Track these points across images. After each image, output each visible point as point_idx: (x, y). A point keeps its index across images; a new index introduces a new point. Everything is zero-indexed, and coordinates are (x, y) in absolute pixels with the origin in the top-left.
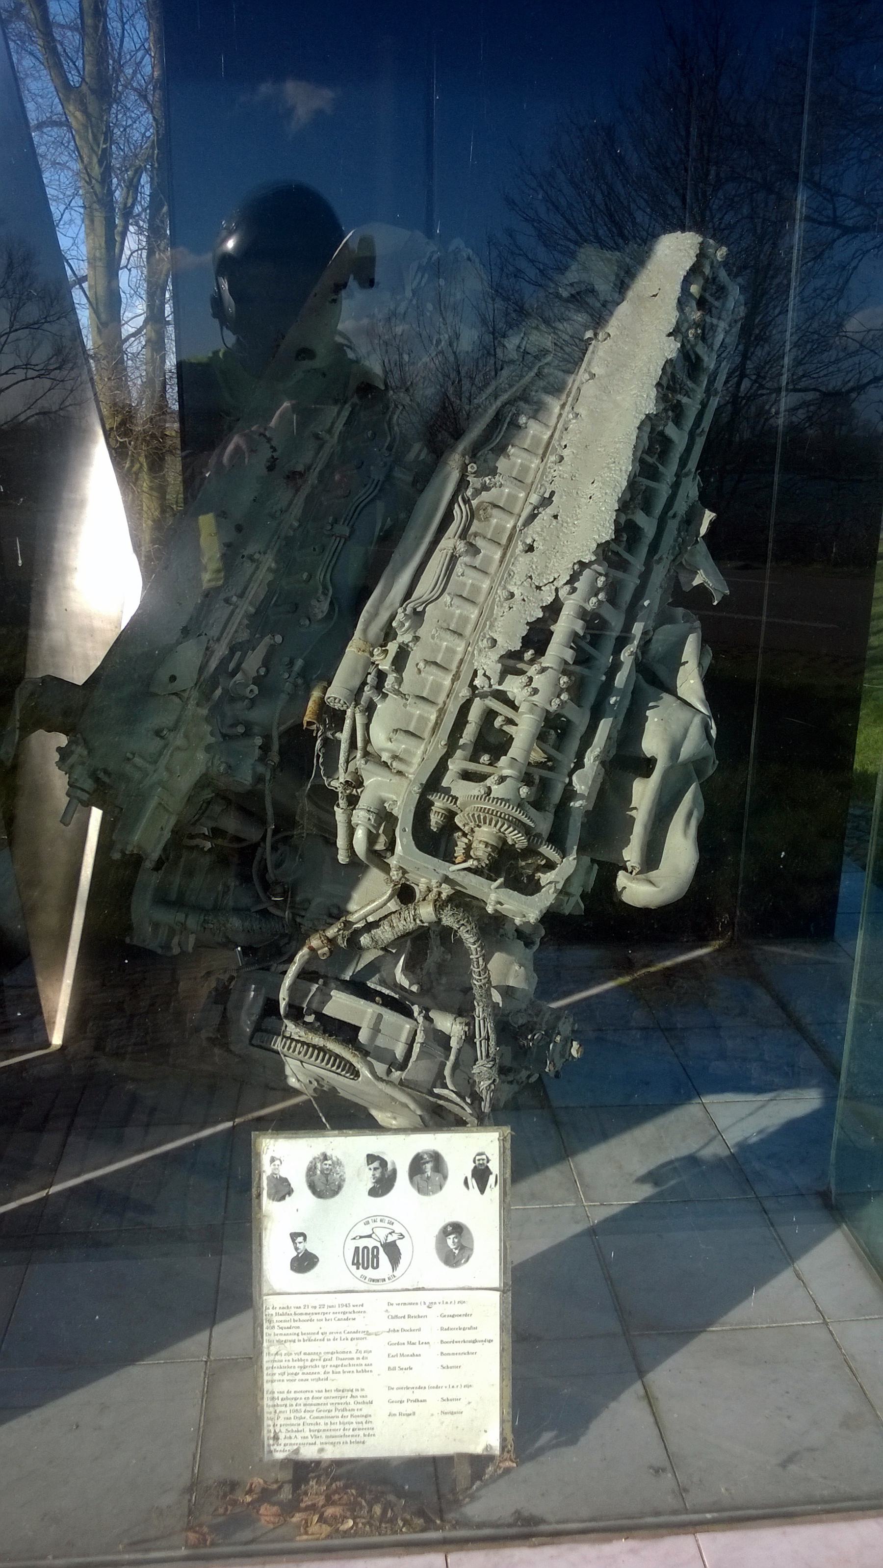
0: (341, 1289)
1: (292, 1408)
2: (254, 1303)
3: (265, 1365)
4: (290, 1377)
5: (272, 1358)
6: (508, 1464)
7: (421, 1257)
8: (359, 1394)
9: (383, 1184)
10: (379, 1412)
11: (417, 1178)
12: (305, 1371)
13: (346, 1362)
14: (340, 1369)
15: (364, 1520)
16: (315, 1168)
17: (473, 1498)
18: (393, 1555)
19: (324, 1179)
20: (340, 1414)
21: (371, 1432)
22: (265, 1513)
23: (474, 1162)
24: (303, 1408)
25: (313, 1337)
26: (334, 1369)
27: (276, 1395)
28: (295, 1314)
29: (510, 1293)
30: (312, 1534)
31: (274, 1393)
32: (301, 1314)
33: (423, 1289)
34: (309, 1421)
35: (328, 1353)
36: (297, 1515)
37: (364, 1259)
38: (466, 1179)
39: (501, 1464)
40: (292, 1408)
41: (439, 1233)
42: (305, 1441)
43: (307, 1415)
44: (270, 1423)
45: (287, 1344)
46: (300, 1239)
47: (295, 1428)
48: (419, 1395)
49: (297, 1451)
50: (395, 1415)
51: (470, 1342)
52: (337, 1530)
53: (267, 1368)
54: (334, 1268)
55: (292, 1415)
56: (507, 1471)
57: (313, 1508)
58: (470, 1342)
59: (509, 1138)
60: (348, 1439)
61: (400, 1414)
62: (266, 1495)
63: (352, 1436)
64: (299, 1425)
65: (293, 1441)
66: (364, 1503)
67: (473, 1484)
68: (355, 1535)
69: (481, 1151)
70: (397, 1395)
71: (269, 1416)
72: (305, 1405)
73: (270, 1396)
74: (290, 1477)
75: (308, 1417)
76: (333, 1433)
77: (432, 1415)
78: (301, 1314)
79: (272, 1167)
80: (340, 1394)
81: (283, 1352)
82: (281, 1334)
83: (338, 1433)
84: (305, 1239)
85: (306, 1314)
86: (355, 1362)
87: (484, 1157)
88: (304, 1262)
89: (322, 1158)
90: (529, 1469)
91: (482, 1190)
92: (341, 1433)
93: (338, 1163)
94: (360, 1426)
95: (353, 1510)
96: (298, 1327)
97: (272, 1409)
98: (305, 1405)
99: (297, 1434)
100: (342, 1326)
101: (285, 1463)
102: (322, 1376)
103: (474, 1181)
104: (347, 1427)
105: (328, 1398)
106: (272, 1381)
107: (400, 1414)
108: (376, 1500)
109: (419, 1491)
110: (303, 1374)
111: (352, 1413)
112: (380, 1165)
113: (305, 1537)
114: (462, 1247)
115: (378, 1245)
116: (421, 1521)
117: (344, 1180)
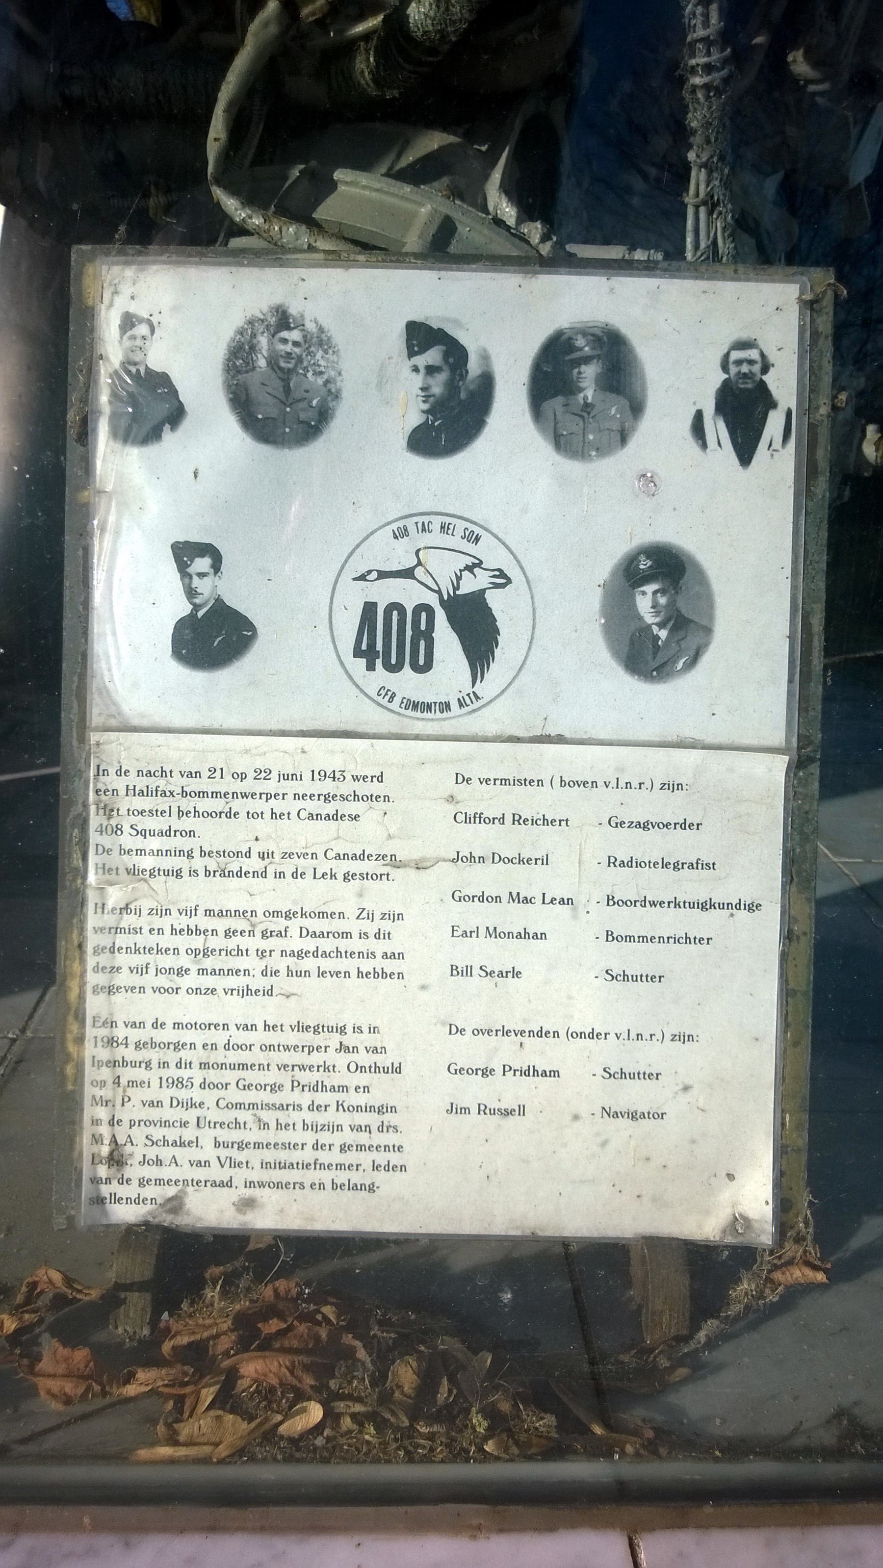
0: (318, 725)
1: (165, 1073)
2: (64, 750)
3: (92, 940)
4: (163, 981)
5: (109, 920)
6: (798, 1274)
7: (557, 630)
8: (366, 1039)
9: (453, 418)
10: (422, 1096)
11: (555, 405)
12: (208, 963)
13: (326, 945)
14: (309, 963)
15: (358, 1408)
16: (253, 348)
17: (699, 1368)
18: (455, 1527)
19: (276, 384)
20: (305, 1099)
21: (395, 1158)
22: (50, 1369)
23: (725, 367)
24: (198, 1076)
25: (234, 866)
26: (291, 961)
27: (120, 1032)
28: (184, 794)
29: (815, 769)
30: (190, 1443)
31: (113, 1024)
32: (202, 794)
33: (560, 739)
34: (214, 1115)
35: (276, 914)
36: (142, 1375)
37: (389, 640)
38: (699, 416)
39: (777, 1276)
40: (165, 1073)
41: (614, 574)
42: (200, 1174)
43: (210, 1097)
44: (102, 1113)
45: (158, 883)
46: (202, 564)
47: (172, 1134)
48: (536, 1053)
49: (175, 1204)
50: (466, 1110)
51: (692, 906)
52: (270, 1436)
53: (97, 951)
54: (305, 652)
55: (165, 1095)
56: (794, 1295)
57: (197, 1356)
58: (692, 906)
59: (828, 301)
60: (326, 1176)
61: (482, 1109)
62: (74, 1320)
63: (340, 1166)
64: (184, 1124)
65: (166, 1173)
66: (362, 1354)
67: (695, 1327)
68: (332, 1453)
69: (744, 335)
70: (472, 1051)
71: (99, 1092)
72: (204, 1066)
73: (103, 1032)
74: (147, 1273)
75: (210, 1101)
76: (283, 1156)
77: (576, 1117)
78: (202, 794)
79: (127, 343)
80: (308, 1038)
81: (146, 904)
82: (140, 852)
83: (296, 1156)
84: (217, 567)
85: (215, 794)
86: (356, 944)
87: (754, 354)
88: (213, 637)
89: (273, 320)
90: (849, 1300)
91: (745, 453)
92: (308, 1155)
93: (320, 340)
94: (363, 1138)
95: (323, 1372)
96: (191, 833)
97: (106, 1073)
98: (204, 1066)
99: (178, 1152)
100: (319, 834)
101: (134, 1235)
102: (258, 982)
103: (722, 426)
104: (325, 1138)
105: (270, 1048)
106: (111, 990)
107: (482, 1109)
108: (405, 1345)
109: (535, 1339)
110: (202, 971)
111: (340, 1096)
112: (446, 355)
113: (165, 1451)
114: (678, 622)
115: (433, 600)
116: (546, 1422)
117: (337, 396)
